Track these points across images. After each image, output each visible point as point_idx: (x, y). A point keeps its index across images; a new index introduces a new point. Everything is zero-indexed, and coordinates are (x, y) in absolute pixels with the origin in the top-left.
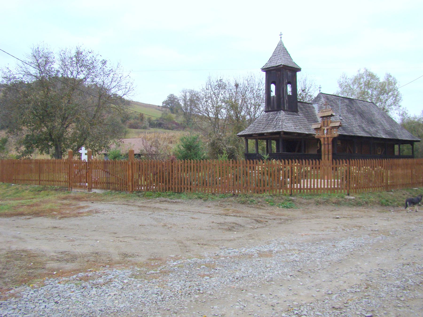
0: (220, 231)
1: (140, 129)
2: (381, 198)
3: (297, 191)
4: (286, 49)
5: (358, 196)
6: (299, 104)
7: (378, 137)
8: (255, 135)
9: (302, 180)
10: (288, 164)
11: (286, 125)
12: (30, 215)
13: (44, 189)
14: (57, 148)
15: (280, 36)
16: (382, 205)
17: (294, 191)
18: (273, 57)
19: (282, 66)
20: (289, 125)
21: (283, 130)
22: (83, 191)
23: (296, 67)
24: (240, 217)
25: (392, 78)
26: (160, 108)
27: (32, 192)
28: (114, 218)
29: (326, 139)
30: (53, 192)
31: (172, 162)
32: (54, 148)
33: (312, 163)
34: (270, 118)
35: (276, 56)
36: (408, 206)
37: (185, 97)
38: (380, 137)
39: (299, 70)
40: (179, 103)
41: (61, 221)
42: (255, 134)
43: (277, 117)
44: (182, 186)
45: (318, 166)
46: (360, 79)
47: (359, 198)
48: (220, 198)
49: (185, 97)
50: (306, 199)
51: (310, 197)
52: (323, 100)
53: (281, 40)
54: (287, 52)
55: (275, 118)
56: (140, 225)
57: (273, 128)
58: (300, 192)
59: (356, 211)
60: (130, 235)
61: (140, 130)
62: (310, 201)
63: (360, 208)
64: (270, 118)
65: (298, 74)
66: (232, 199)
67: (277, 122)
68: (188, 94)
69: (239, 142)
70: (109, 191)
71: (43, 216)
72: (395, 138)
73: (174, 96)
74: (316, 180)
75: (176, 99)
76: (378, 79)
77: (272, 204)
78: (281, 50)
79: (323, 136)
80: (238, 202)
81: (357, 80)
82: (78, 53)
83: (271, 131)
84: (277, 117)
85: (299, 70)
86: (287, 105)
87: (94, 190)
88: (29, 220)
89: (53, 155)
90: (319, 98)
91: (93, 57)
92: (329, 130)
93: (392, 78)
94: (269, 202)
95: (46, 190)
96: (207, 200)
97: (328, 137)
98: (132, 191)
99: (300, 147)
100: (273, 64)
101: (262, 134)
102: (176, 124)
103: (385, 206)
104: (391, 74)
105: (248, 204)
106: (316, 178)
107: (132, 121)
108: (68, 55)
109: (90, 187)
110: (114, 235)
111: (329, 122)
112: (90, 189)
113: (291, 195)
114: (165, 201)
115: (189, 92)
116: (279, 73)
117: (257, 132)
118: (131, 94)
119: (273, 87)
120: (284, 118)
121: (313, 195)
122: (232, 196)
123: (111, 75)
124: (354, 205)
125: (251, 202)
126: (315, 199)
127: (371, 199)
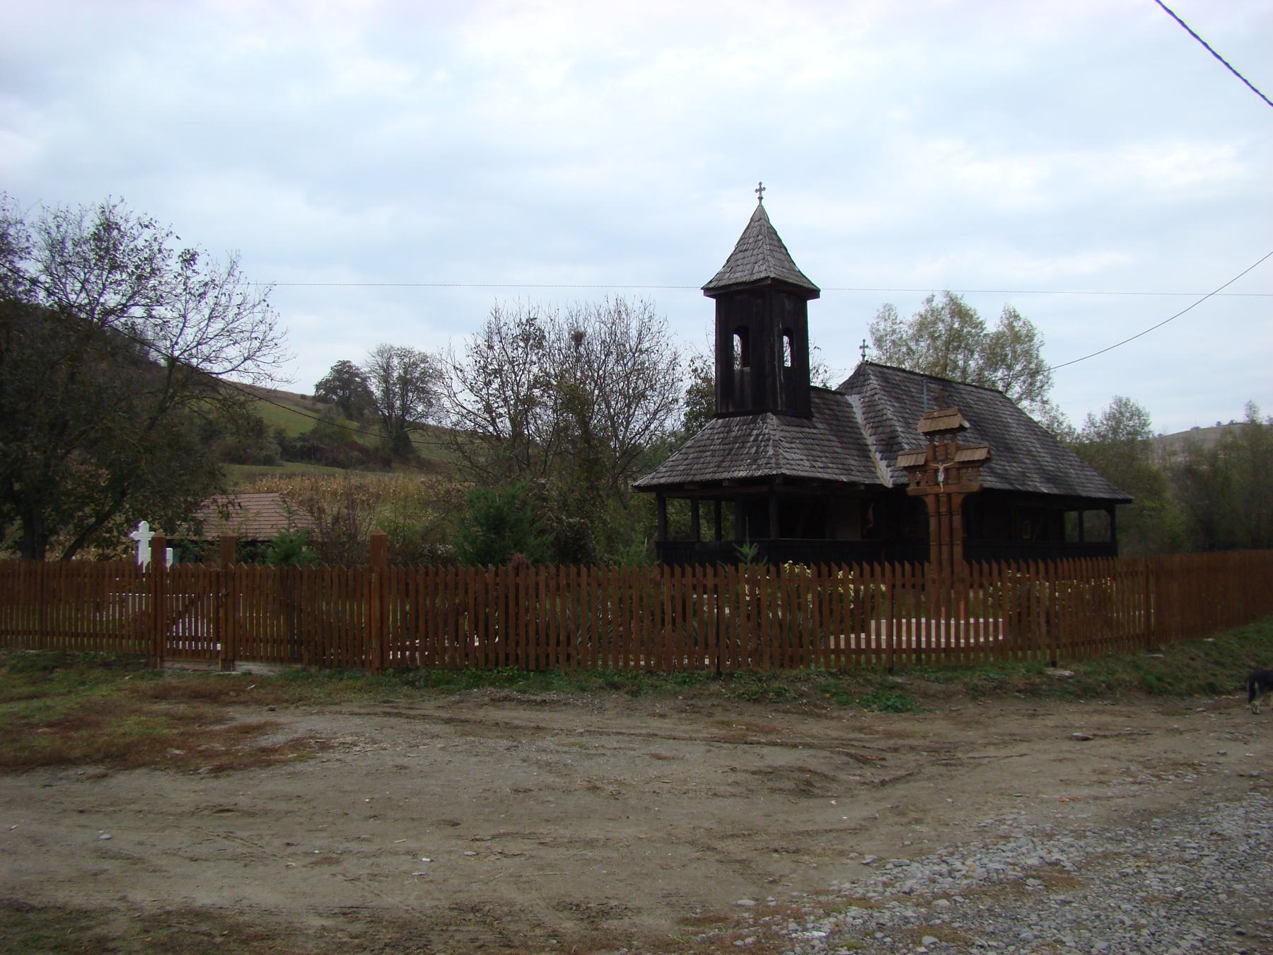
0: (776, 796)
1: (253, 464)
3: (909, 658)
4: (776, 233)
5: (1082, 668)
7: (1031, 489)
9: (873, 622)
10: (883, 574)
14: (28, 525)
18: (741, 255)
21: (784, 471)
22: (204, 667)
24: (795, 746)
25: (1021, 323)
26: (309, 403)
27: (21, 671)
28: (406, 768)
29: (944, 499)
30: (97, 672)
31: (517, 575)
34: (733, 434)
35: (749, 253)
36: (1258, 693)
37: (387, 369)
39: (814, 293)
41: (223, 783)
42: (691, 482)
43: (755, 432)
44: (550, 650)
46: (934, 323)
47: (1085, 673)
49: (387, 369)
50: (937, 680)
51: (949, 674)
52: (874, 382)
54: (780, 240)
55: (750, 435)
56: (517, 791)
58: (919, 659)
59: (1112, 714)
60: (510, 829)
61: (254, 468)
62: (952, 687)
63: (1095, 704)
64: (733, 434)
65: (811, 304)
66: (715, 687)
67: (758, 447)
68: (395, 361)
69: (594, 505)
70: (299, 666)
72: (1070, 492)
73: (350, 367)
74: (914, 620)
75: (357, 375)
76: (979, 326)
77: (844, 698)
78: (760, 234)
79: (935, 490)
80: (739, 696)
81: (925, 326)
82: (108, 226)
83: (742, 474)
84: (755, 432)
85: (814, 293)
87: (243, 667)
88: (104, 783)
89: (18, 546)
91: (155, 239)
92: (953, 472)
93: (1021, 323)
94: (833, 695)
95: (71, 666)
97: (948, 490)
99: (811, 521)
100: (741, 276)
102: (363, 450)
103: (1160, 694)
104: (1019, 312)
105: (771, 701)
108: (72, 232)
109: (231, 654)
110: (450, 830)
111: (952, 449)
112: (228, 662)
113: (890, 671)
114: (506, 699)
115: (399, 356)
117: (698, 478)
118: (270, 359)
120: (778, 435)
121: (955, 669)
122: (714, 679)
123: (210, 299)
124: (1079, 697)
125: (779, 694)
126: (965, 680)
127: (1118, 676)
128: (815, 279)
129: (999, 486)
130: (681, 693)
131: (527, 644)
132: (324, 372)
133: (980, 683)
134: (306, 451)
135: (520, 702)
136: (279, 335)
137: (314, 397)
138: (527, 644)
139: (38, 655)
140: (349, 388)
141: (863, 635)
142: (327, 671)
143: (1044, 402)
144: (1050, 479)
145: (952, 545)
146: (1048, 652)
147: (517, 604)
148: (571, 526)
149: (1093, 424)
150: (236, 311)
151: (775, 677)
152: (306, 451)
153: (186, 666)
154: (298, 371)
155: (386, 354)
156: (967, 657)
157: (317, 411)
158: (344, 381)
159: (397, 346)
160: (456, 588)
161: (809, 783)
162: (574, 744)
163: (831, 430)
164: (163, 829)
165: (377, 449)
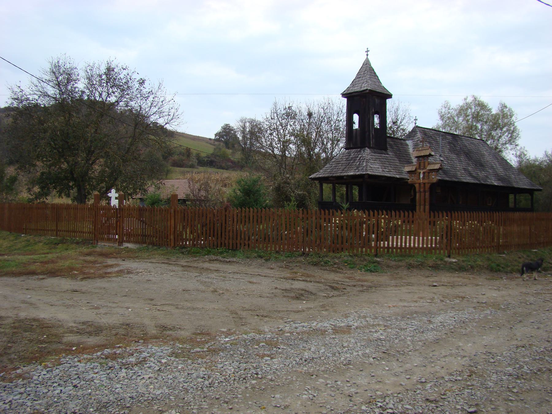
0: (285, 299)
2: (490, 262)
3: (384, 251)
4: (373, 70)
6: (388, 140)
7: (489, 183)
8: (332, 179)
9: (391, 237)
10: (374, 215)
11: (371, 166)
12: (44, 274)
13: (62, 242)
14: (79, 190)
15: (366, 53)
16: (491, 270)
17: (380, 250)
18: (357, 80)
19: (368, 91)
20: (375, 166)
21: (368, 172)
22: (111, 245)
23: (386, 93)
25: (507, 109)
26: (212, 142)
27: (47, 245)
29: (422, 185)
31: (226, 211)
32: (75, 189)
35: (361, 79)
37: (244, 127)
39: (390, 96)
40: (236, 136)
41: (83, 283)
42: (332, 177)
43: (360, 156)
44: (238, 242)
46: (467, 109)
48: (286, 257)
49: (244, 127)
50: (395, 260)
52: (419, 135)
53: (367, 58)
54: (375, 73)
55: (357, 157)
57: (356, 170)
58: (388, 251)
59: (458, 277)
62: (400, 263)
63: (464, 274)
65: (388, 101)
66: (302, 259)
67: (360, 162)
68: (248, 124)
69: (312, 186)
71: (60, 276)
72: (509, 185)
73: (230, 127)
75: (232, 130)
76: (490, 110)
77: (352, 266)
78: (367, 70)
79: (419, 181)
80: (309, 263)
81: (462, 111)
83: (352, 173)
84: (360, 156)
85: (390, 96)
86: (374, 140)
87: (126, 245)
90: (414, 133)
91: (128, 74)
92: (426, 174)
93: (507, 109)
94: (348, 264)
95: (65, 243)
96: (269, 259)
98: (174, 247)
99: (381, 193)
100: (357, 89)
101: (341, 178)
103: (496, 271)
104: (507, 104)
105: (322, 265)
106: (434, 235)
107: (176, 157)
108: (96, 72)
110: (150, 302)
111: (426, 164)
112: (121, 242)
113: (376, 256)
114: (216, 260)
115: (249, 122)
116: (364, 99)
117: (334, 175)
118: (176, 123)
119: (356, 117)
120: (369, 157)
121: (404, 256)
122: (301, 256)
123: (151, 99)
124: (456, 270)
125: (326, 263)
127: (478, 262)
128: (390, 90)
129: (472, 181)
130: (285, 260)
131: (229, 239)
132: (218, 129)
133: (413, 263)
134: (210, 162)
135: (221, 261)
136: (180, 113)
137: (215, 140)
138: (229, 239)
139: (54, 239)
140: (229, 135)
141: (386, 243)
142: (155, 247)
143: (517, 145)
144: (500, 179)
145: (425, 205)
146: (446, 252)
147: (226, 223)
148: (298, 194)
149: (547, 156)
150: (161, 104)
151: (327, 256)
152: (210, 162)
153: (106, 244)
154: (208, 129)
155: (244, 121)
156: (410, 252)
157: (214, 145)
158: (226, 133)
159: (248, 118)
160: (203, 216)
161: (302, 295)
162: (221, 276)
163: (396, 155)
164: (49, 296)
165: (239, 162)
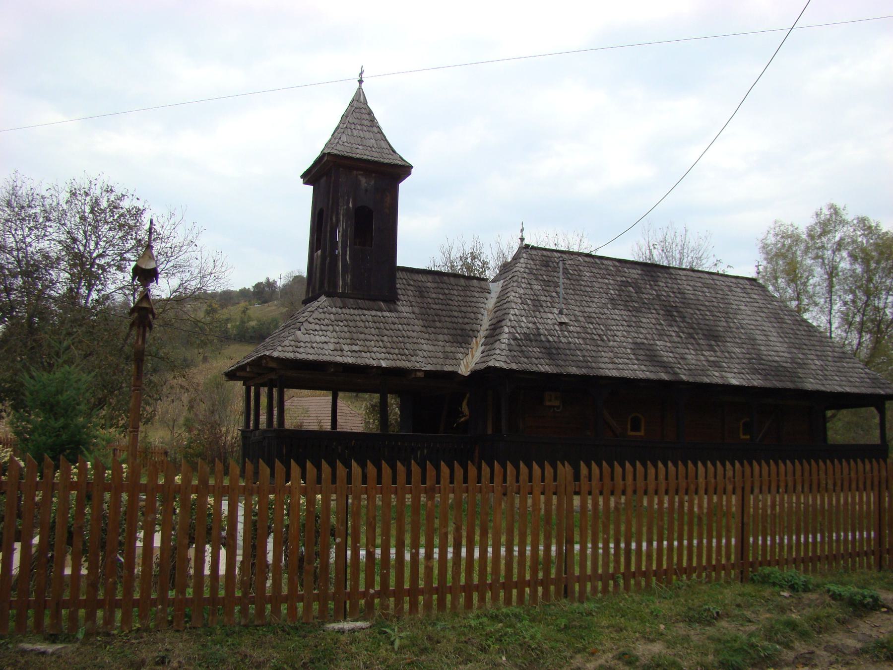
33: (349, 475)
38: (720, 381)
39: (404, 170)
45: (683, 484)
53: (360, 89)
78: (359, 114)
85: (404, 170)
86: (349, 278)
